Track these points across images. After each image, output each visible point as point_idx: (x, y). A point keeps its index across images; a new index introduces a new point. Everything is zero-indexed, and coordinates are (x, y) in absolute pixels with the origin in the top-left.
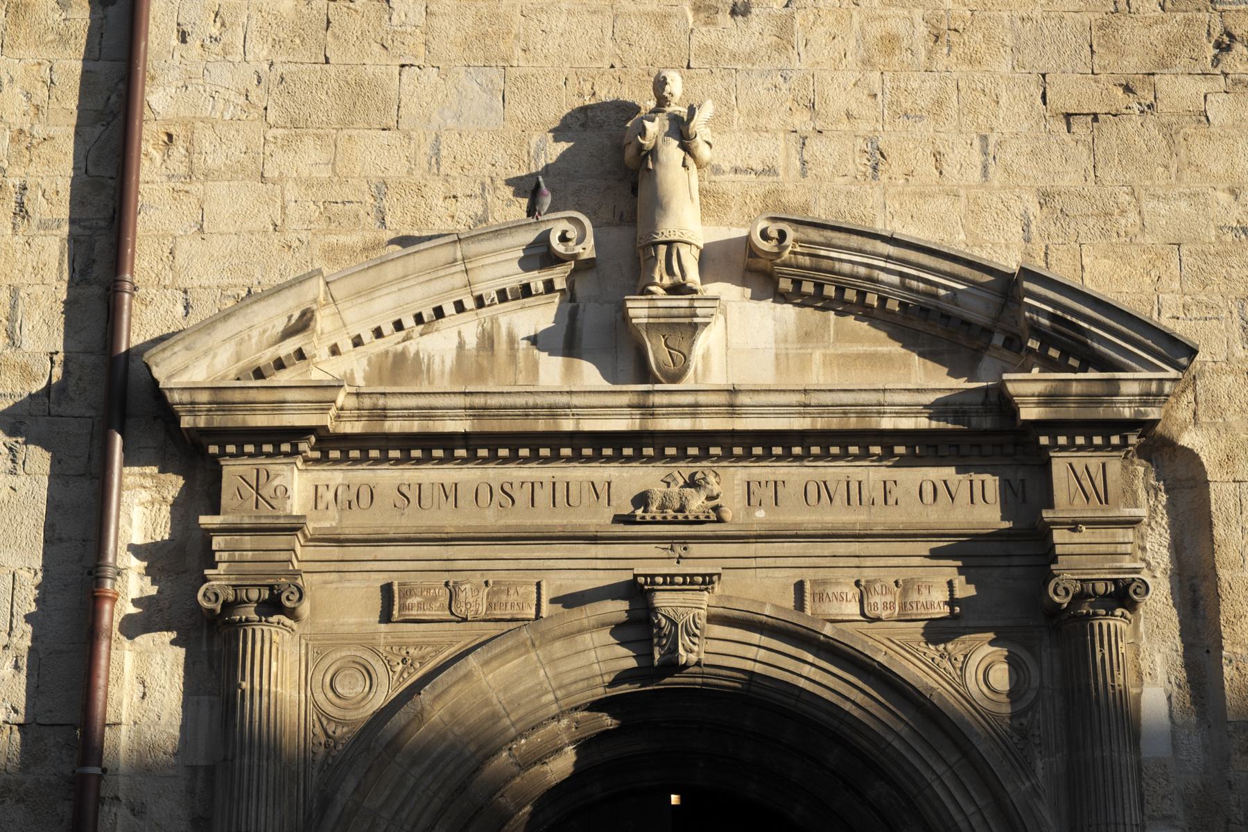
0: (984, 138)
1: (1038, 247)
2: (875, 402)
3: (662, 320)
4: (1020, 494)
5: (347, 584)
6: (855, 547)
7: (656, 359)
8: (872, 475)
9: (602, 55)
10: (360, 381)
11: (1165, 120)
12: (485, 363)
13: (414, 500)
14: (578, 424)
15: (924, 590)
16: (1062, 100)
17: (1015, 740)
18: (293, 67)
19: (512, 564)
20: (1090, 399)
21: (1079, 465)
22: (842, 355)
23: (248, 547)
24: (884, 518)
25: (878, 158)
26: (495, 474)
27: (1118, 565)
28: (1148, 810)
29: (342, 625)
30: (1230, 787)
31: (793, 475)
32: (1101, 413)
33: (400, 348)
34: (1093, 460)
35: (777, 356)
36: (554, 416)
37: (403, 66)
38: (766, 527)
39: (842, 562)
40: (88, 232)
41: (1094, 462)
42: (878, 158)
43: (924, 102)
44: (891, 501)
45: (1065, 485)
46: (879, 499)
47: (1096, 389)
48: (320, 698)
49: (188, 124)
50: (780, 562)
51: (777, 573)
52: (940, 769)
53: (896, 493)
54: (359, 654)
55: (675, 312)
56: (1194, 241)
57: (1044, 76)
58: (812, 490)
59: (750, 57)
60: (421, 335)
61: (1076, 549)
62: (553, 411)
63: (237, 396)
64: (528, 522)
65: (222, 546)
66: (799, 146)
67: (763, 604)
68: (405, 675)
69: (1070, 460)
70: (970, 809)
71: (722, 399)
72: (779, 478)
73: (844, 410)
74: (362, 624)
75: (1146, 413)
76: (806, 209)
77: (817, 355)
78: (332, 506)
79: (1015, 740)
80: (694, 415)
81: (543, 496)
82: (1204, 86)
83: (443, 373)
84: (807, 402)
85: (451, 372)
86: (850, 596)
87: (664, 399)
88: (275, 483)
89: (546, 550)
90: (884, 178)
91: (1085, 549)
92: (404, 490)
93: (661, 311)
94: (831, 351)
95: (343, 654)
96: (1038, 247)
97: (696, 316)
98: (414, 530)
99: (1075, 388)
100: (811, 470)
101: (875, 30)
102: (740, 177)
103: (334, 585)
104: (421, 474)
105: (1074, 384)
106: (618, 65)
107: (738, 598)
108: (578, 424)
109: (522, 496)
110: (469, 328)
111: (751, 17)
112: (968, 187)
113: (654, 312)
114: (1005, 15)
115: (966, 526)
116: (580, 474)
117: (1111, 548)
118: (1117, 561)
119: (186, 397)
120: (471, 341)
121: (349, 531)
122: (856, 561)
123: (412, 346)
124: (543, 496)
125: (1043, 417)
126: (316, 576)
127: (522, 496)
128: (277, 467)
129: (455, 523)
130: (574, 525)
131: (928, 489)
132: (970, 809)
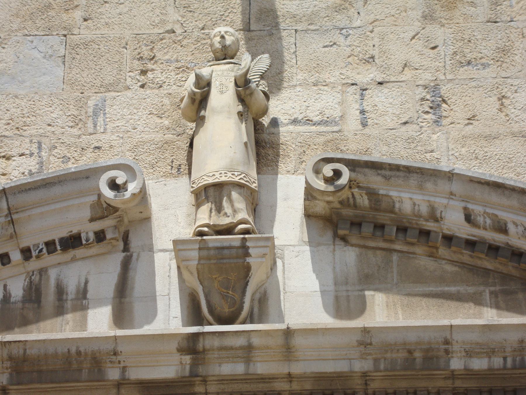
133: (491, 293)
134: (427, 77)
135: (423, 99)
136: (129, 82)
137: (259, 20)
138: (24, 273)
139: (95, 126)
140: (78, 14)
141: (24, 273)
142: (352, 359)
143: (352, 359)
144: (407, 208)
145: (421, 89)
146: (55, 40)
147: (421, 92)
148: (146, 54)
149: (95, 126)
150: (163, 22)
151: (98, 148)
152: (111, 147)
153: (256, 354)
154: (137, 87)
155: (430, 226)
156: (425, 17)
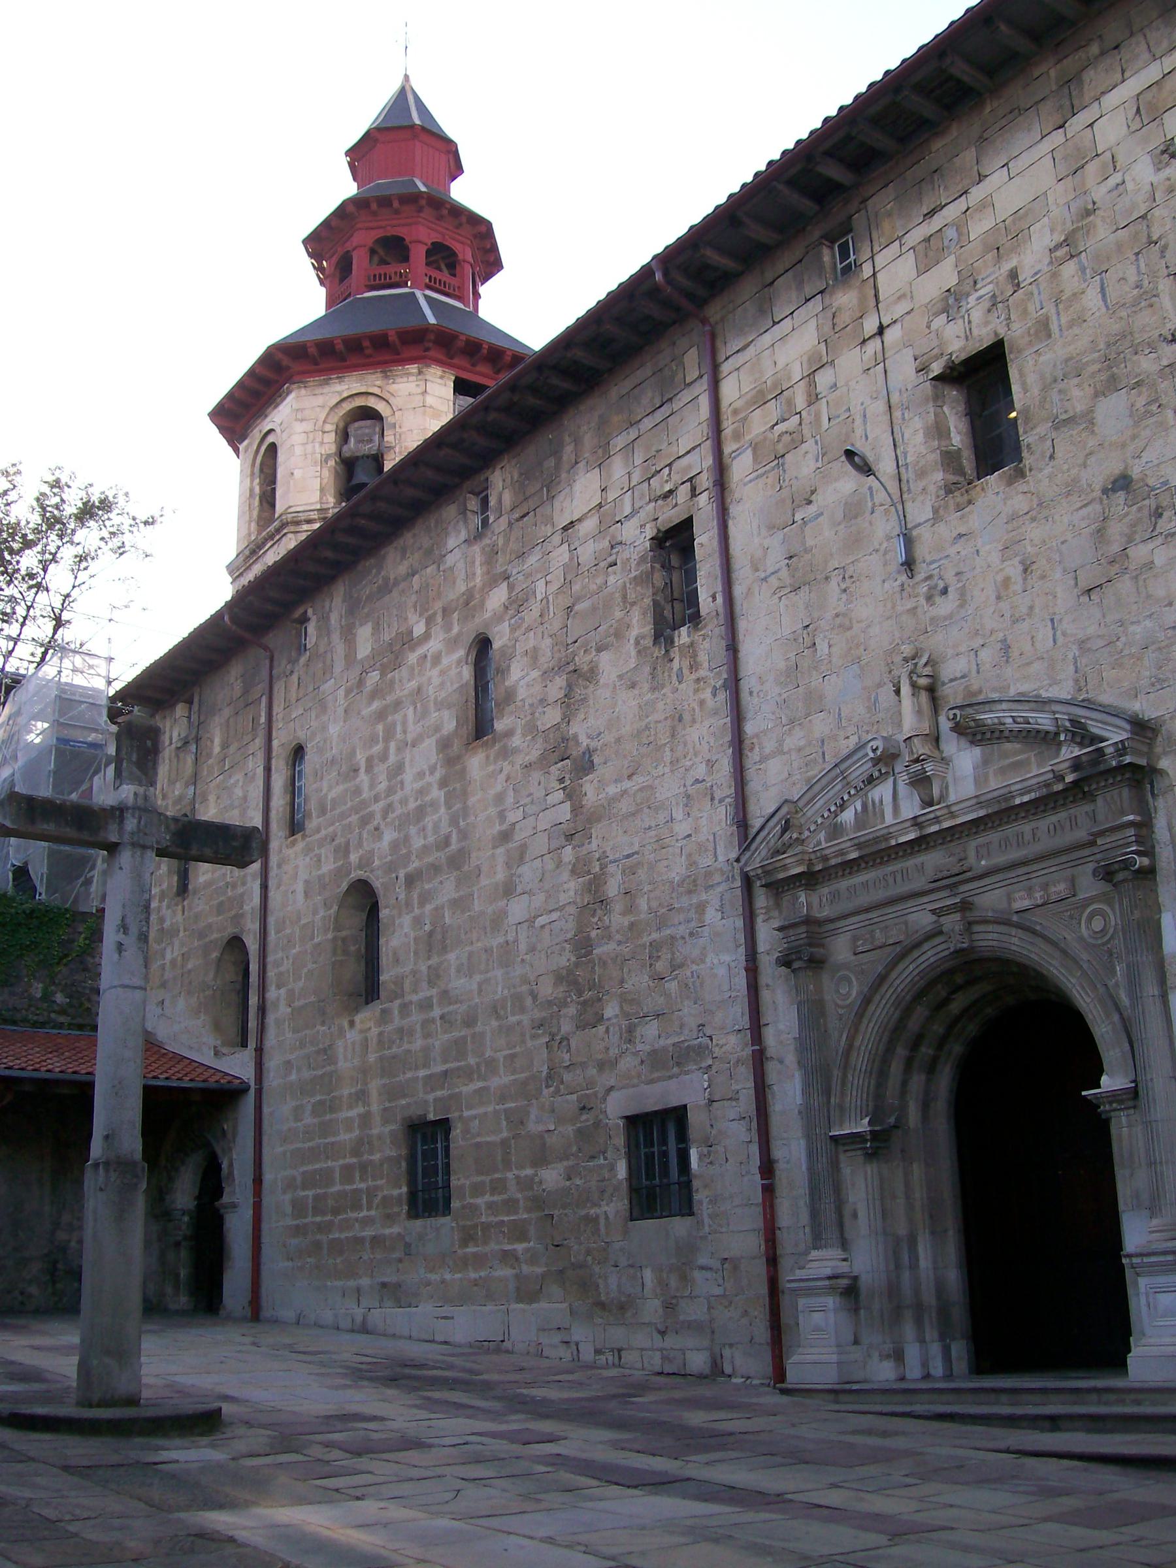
0: (1052, 620)
8: (1026, 828)
11: (1134, 574)
16: (1084, 584)
31: (993, 837)
32: (1102, 767)
47: (1094, 756)
51: (996, 891)
56: (1153, 643)
59: (950, 616)
63: (770, 868)
71: (974, 801)
73: (997, 800)
75: (1123, 761)
77: (991, 771)
101: (999, 578)
104: (284, 1010)
111: (949, 593)
116: (911, 863)
120: (859, 808)
122: (1027, 877)
131: (1052, 827)
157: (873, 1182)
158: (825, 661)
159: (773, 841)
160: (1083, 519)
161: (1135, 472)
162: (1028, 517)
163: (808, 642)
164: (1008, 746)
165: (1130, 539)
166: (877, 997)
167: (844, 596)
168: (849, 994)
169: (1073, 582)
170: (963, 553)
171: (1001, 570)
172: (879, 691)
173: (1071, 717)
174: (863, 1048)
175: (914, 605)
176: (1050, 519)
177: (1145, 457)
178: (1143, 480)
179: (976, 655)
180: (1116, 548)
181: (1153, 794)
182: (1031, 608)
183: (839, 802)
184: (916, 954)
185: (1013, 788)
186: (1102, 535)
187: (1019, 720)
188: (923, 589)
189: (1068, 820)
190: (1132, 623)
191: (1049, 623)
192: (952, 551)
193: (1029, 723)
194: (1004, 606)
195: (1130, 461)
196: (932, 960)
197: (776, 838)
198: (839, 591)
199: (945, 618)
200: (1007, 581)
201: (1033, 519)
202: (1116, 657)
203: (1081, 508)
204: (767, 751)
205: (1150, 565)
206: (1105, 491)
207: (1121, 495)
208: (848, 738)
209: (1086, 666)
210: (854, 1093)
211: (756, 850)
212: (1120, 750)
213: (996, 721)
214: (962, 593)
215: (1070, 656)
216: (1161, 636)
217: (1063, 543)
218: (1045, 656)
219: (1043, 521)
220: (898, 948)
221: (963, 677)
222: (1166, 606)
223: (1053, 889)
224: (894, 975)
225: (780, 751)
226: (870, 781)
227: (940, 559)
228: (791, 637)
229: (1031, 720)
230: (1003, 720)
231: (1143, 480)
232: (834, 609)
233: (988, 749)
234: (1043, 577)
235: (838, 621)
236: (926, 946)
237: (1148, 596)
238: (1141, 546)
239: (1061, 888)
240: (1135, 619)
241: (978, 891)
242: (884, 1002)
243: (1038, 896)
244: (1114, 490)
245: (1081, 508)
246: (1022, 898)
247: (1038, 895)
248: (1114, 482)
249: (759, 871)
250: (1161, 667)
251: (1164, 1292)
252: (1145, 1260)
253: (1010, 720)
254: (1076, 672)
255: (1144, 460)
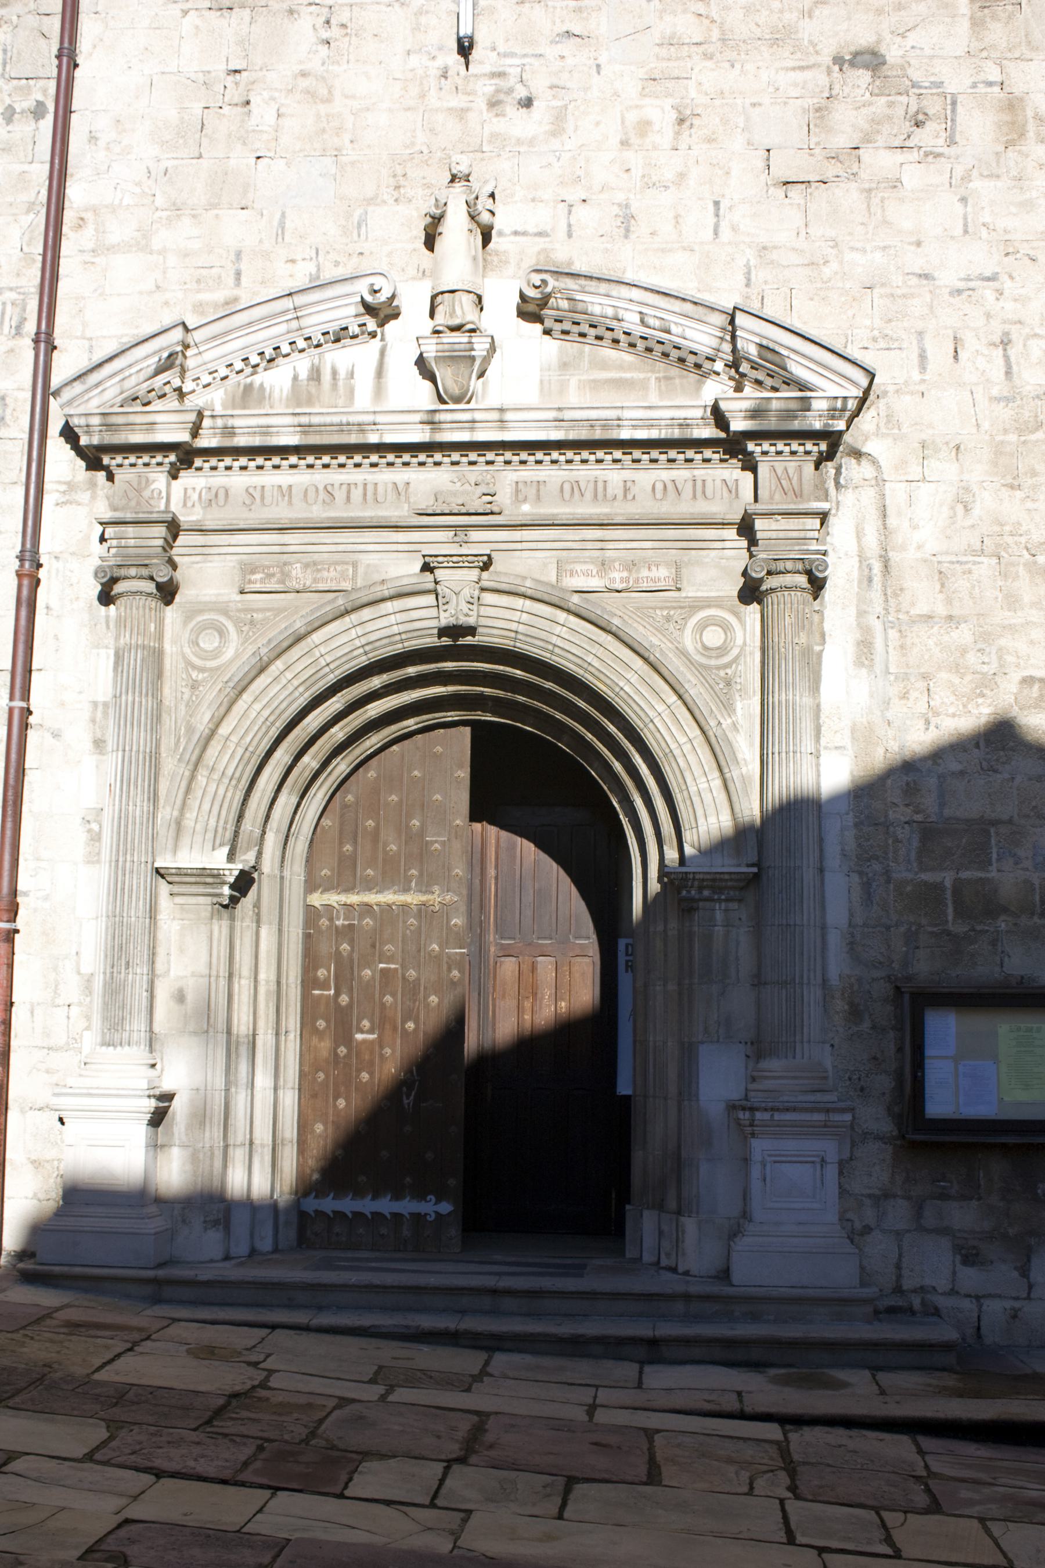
0: (717, 204)
1: (754, 292)
2: (615, 417)
3: (447, 354)
4: (734, 491)
5: (209, 564)
6: (598, 533)
7: (443, 385)
9: (413, 144)
10: (219, 410)
11: (867, 186)
12: (313, 391)
13: (258, 499)
14: (381, 437)
15: (654, 568)
16: (781, 172)
17: (721, 686)
18: (176, 162)
19: (333, 548)
20: (788, 414)
21: (779, 467)
22: (594, 381)
23: (131, 536)
24: (621, 510)
25: (627, 221)
26: (320, 477)
27: (805, 547)
28: (823, 741)
29: (205, 595)
30: (889, 724)
33: (249, 380)
34: (793, 464)
35: (541, 382)
36: (363, 431)
37: (258, 158)
38: (529, 517)
39: (589, 545)
40: (22, 297)
41: (792, 466)
42: (627, 221)
43: (669, 175)
44: (630, 497)
45: (767, 484)
46: (620, 496)
47: (793, 405)
48: (187, 650)
49: (95, 210)
50: (540, 545)
52: (661, 707)
53: (635, 490)
54: (216, 617)
55: (457, 347)
56: (883, 285)
57: (768, 151)
58: (567, 487)
59: (531, 142)
60: (265, 370)
61: (774, 535)
62: (361, 427)
63: (120, 420)
64: (345, 515)
65: (112, 536)
66: (566, 212)
67: (525, 578)
68: (251, 634)
69: (772, 464)
70: (682, 740)
71: (495, 416)
72: (541, 479)
74: (219, 595)
75: (832, 425)
76: (570, 263)
77: (574, 382)
78: (197, 504)
79: (721, 686)
80: (472, 429)
81: (357, 494)
82: (900, 157)
83: (281, 400)
84: (561, 418)
85: (288, 399)
86: (594, 572)
87: (448, 417)
88: (153, 487)
89: (359, 537)
90: (633, 236)
91: (781, 535)
92: (251, 490)
93: (446, 347)
94: (584, 377)
95: (205, 617)
96: (754, 292)
97: (473, 349)
98: (258, 521)
99: (775, 405)
100: (567, 472)
101: (632, 117)
102: (518, 238)
103: (200, 565)
105: (774, 402)
106: (426, 151)
107: (506, 574)
108: (381, 437)
109: (340, 495)
110: (302, 364)
112: (702, 243)
113: (440, 347)
114: (739, 101)
115: (688, 516)
116: (399, 475)
117: (802, 534)
118: (805, 544)
119: (82, 421)
120: (303, 375)
121: (210, 525)
122: (599, 545)
123: (257, 379)
124: (357, 494)
125: (754, 428)
126: (186, 558)
127: (340, 495)
128: (155, 475)
129: (290, 516)
130: (379, 517)
131: (659, 487)
132: (682, 740)
133: (656, 378)
134: (620, 197)
135: (616, 216)
136: (385, 197)
137: (490, 142)
138: (1005, 1554)
139: (359, 235)
140: (347, 137)
141: (1005, 1554)
142: (984, 1296)
143: (984, 1296)
144: (597, 310)
145: (615, 207)
146: (328, 161)
147: (616, 210)
148: (399, 171)
149: (359, 235)
150: (413, 144)
151: (361, 254)
152: (371, 253)
153: (695, 838)
154: (391, 201)
155: (614, 324)
156: (622, 143)
157: (219, 952)
158: (265, 137)
159: (133, 381)
160: (796, 85)
161: (893, 53)
162: (700, 49)
163: (235, 95)
164: (609, 353)
165: (868, 139)
166: (279, 665)
167: (324, 50)
168: (216, 654)
169: (761, 164)
170: (570, 61)
171: (637, 106)
172: (370, 209)
173: (765, 342)
174: (234, 739)
175: (464, 105)
176: (738, 66)
177: (912, 39)
178: (903, 68)
179: (570, 212)
180: (842, 141)
181: (837, 484)
182: (682, 176)
183: (269, 353)
184: (366, 613)
185: (627, 414)
186: (822, 117)
187: (651, 321)
188: (486, 88)
189: (690, 484)
190: (852, 249)
191: (711, 207)
192: (552, 52)
193: (668, 332)
194: (634, 159)
195: (888, 37)
196: (396, 629)
197: (142, 376)
198: (314, 40)
199: (519, 142)
200: (644, 127)
201: (708, 56)
202: (819, 286)
203: (794, 69)
204: (113, 238)
205: (896, 184)
206: (838, 60)
207: (863, 77)
208: (293, 261)
209: (766, 282)
210: (206, 806)
211: (97, 385)
212: (835, 410)
213: (610, 312)
214: (559, 118)
215: (741, 262)
216: (897, 279)
217: (754, 105)
218: (696, 248)
219: (727, 65)
220: (341, 601)
221: (540, 234)
222: (910, 244)
223: (645, 573)
224: (317, 637)
225: (142, 244)
226: (340, 336)
227: (525, 56)
228: (201, 78)
229: (674, 329)
230: (621, 314)
231: (903, 68)
232: (301, 62)
233: (572, 348)
234: (710, 140)
235: (304, 83)
236: (389, 606)
237: (885, 222)
238: (883, 153)
239: (662, 574)
240: (859, 245)
241: (519, 546)
242: (289, 675)
243: (617, 577)
244: (852, 64)
245: (794, 69)
246: (588, 574)
247: (616, 575)
248: (856, 54)
249: (96, 421)
250: (890, 320)
251: (789, 1162)
252: (777, 1116)
253: (636, 318)
254: (748, 285)
255: (910, 42)
